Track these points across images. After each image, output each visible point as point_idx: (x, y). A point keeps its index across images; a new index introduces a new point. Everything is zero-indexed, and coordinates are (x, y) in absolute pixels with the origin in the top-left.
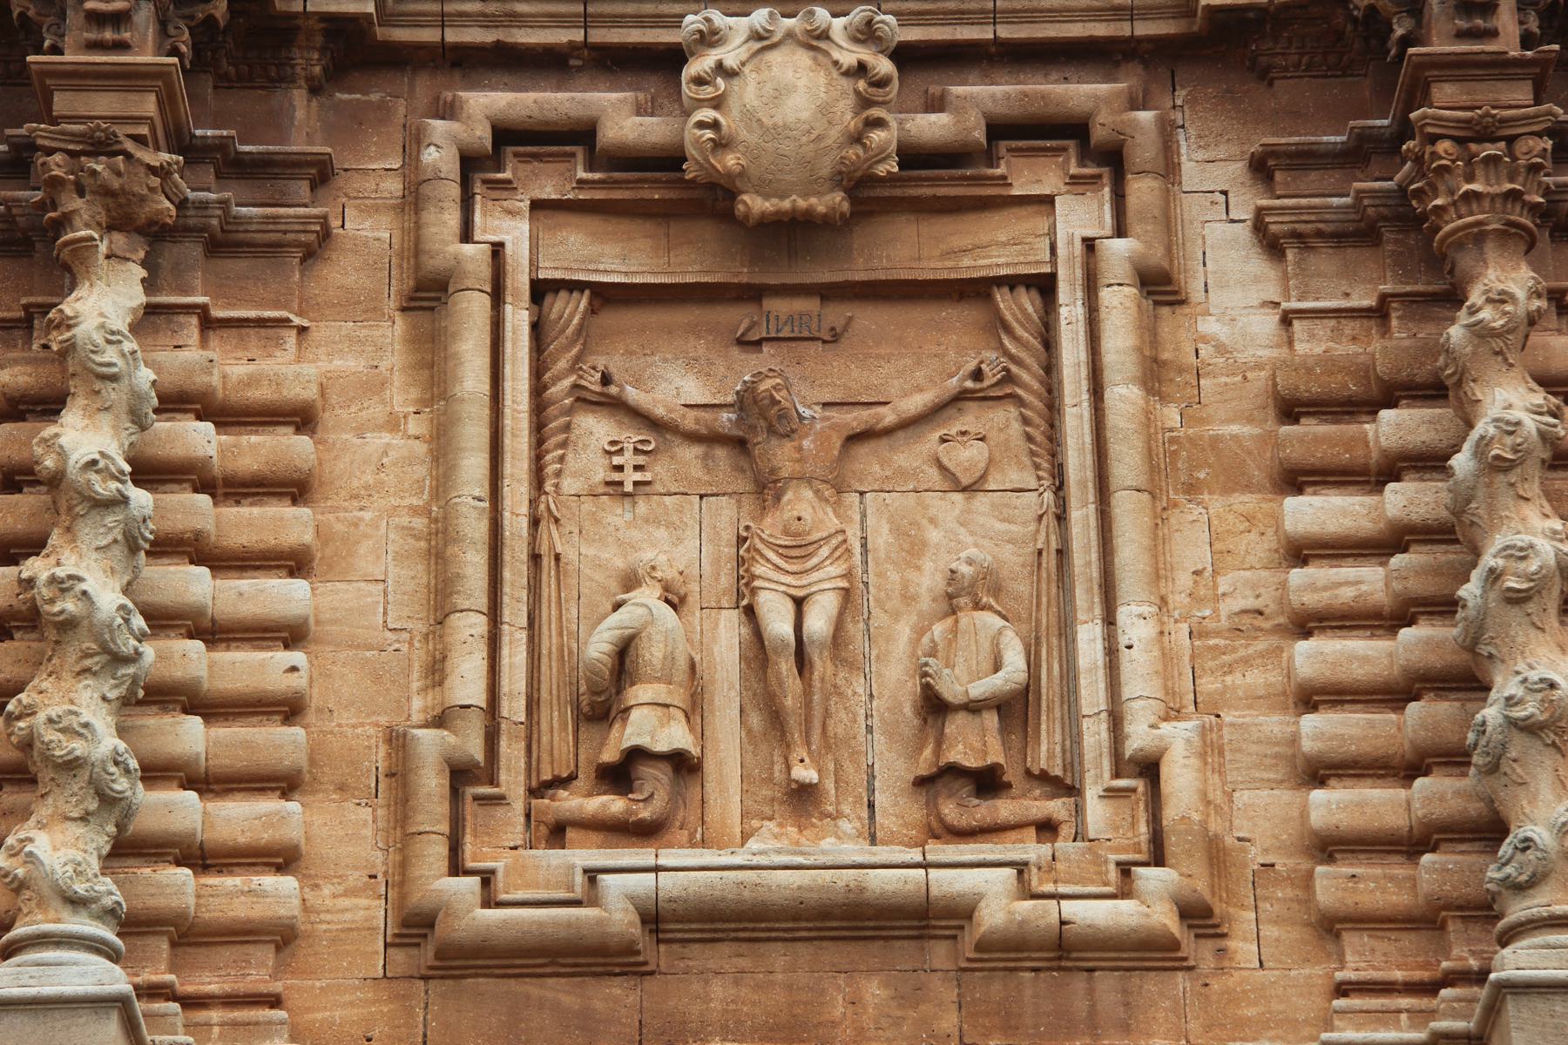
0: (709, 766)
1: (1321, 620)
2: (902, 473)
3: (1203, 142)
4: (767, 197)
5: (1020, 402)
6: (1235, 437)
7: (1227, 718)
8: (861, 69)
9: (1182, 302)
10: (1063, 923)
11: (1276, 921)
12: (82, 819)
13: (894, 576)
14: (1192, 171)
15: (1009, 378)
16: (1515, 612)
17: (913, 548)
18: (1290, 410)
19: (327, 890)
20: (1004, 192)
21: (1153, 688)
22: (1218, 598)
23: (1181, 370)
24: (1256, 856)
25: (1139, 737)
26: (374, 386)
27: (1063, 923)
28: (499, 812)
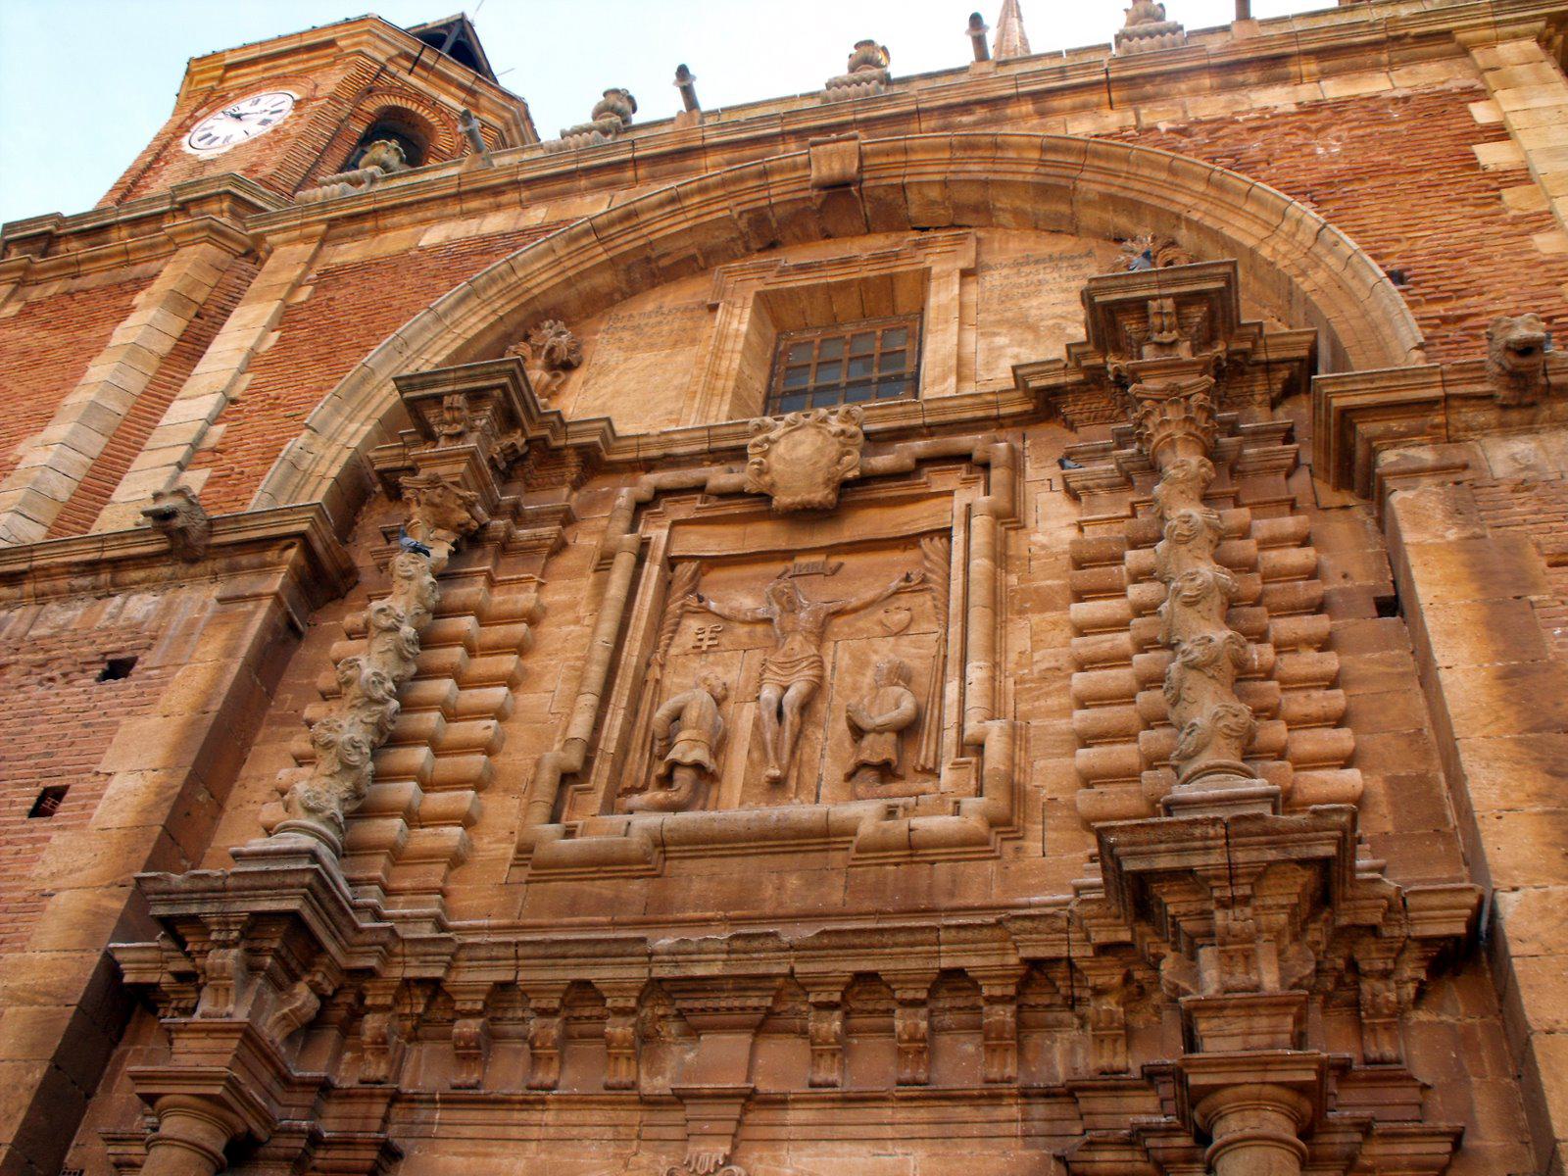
0: (725, 781)
1: (1092, 663)
2: (861, 630)
3: (1038, 460)
4: (789, 496)
5: (931, 589)
6: (1050, 587)
7: (1034, 723)
8: (843, 432)
9: (1024, 527)
10: (910, 830)
11: (1055, 829)
12: (331, 776)
13: (848, 679)
14: (1031, 470)
15: (924, 580)
16: (1189, 611)
17: (861, 663)
18: (1079, 564)
19: (485, 841)
20: (927, 491)
21: (984, 703)
22: (1033, 664)
23: (1019, 559)
24: (1045, 794)
25: (972, 727)
26: (572, 606)
27: (910, 830)
28: (590, 797)
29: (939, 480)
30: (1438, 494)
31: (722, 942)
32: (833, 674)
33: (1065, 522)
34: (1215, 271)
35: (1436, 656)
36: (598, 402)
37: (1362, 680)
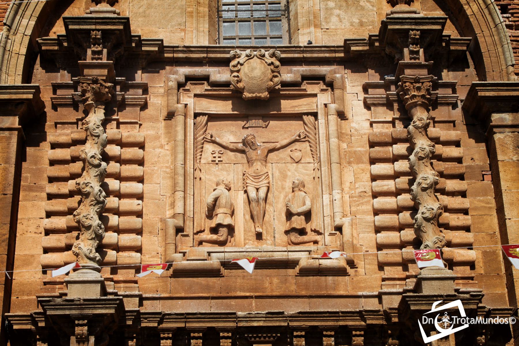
2: (281, 159)
6: (359, 151)
10: (320, 265)
11: (369, 264)
13: (280, 183)
18: (372, 145)
29: (311, 89)
30: (512, 137)
31: (263, 314)
32: (273, 180)
33: (364, 118)
34: (439, 21)
35: (506, 213)
36: (141, 10)
37: (476, 209)
